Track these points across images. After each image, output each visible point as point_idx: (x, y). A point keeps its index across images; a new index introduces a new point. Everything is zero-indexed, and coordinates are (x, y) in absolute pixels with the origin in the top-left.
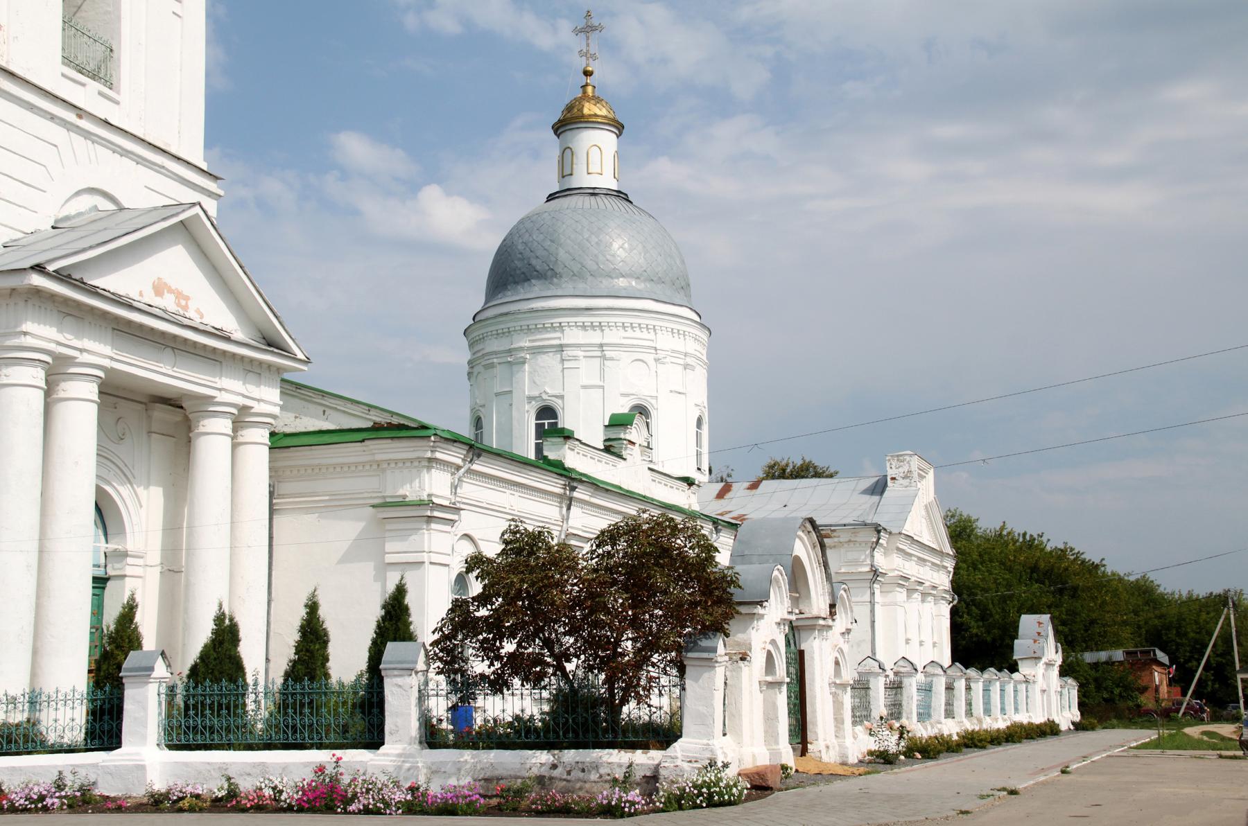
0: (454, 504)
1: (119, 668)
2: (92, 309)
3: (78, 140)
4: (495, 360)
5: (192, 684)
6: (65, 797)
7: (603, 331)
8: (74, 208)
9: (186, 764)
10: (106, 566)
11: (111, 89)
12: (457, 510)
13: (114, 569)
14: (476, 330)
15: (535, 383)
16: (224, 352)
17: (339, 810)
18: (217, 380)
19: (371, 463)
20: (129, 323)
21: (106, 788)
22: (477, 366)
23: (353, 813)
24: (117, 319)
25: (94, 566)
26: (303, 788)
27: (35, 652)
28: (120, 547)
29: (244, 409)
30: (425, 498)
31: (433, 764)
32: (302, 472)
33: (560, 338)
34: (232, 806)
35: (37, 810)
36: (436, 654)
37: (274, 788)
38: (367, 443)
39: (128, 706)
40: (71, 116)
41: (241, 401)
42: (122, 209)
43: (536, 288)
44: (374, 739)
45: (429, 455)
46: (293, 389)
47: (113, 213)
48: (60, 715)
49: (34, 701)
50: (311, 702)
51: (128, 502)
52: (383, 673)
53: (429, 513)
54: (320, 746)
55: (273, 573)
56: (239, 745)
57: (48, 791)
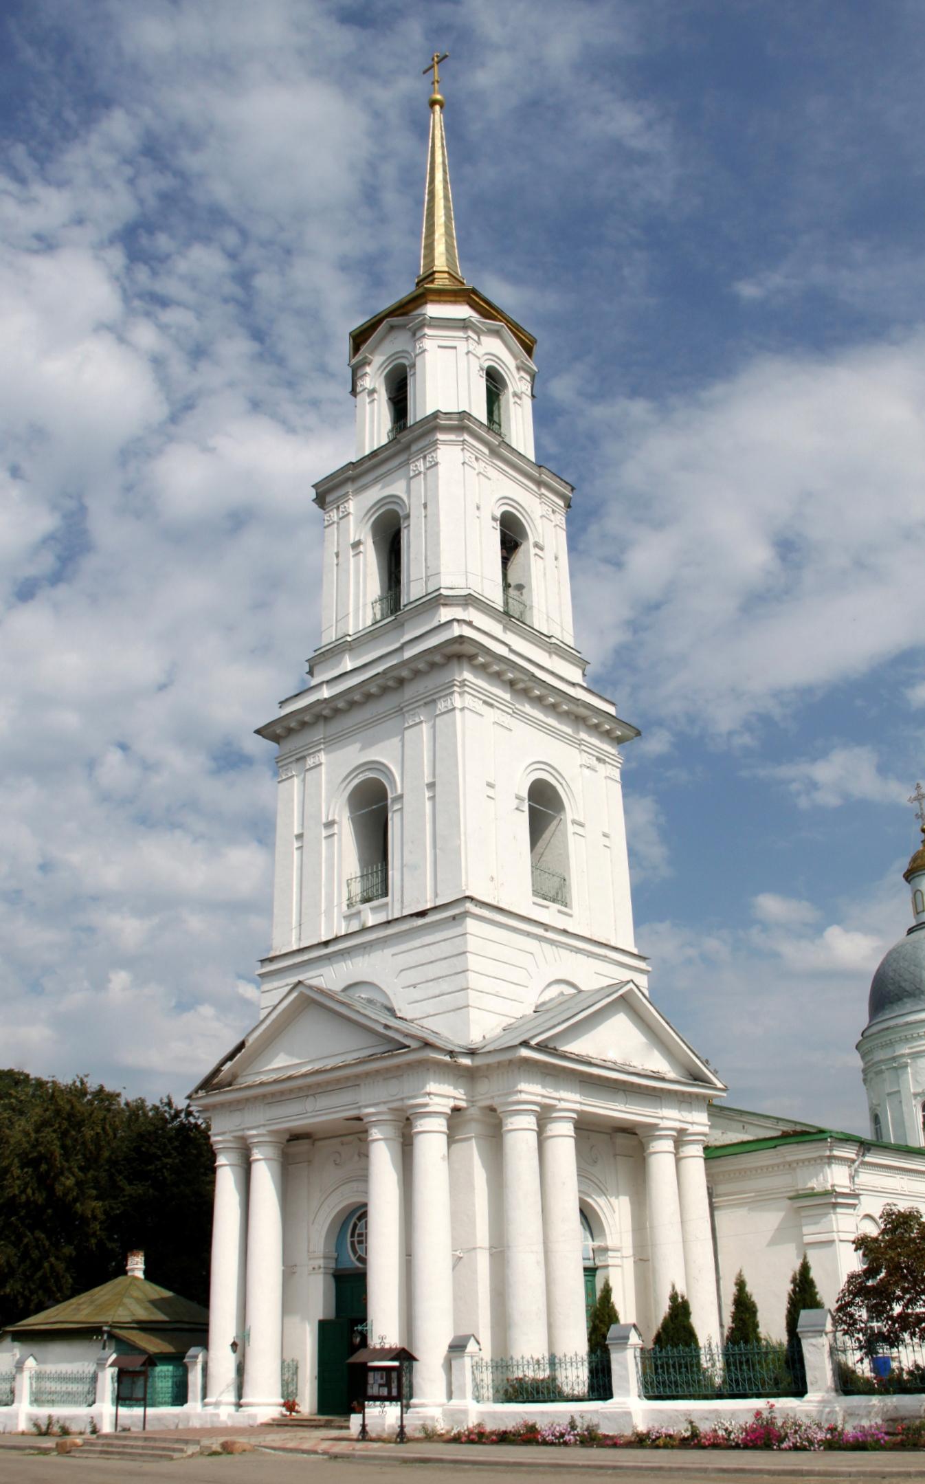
0: (854, 1191)
1: (604, 1337)
2: (564, 1069)
3: (546, 946)
4: (883, 1067)
5: (658, 1349)
6: (578, 1435)
8: (546, 996)
9: (661, 1411)
10: (594, 1259)
11: (566, 907)
12: (857, 1196)
13: (600, 1261)
14: (865, 1045)
15: (917, 1081)
16: (662, 1090)
17: (775, 1447)
18: (659, 1111)
19: (784, 1164)
20: (591, 1075)
21: (605, 1429)
22: (870, 1073)
23: (785, 1449)
24: (582, 1073)
25: (584, 1259)
26: (746, 1430)
27: (550, 1327)
28: (603, 1244)
29: (682, 1132)
30: (830, 1188)
31: (848, 1408)
32: (732, 1175)
34: (695, 1444)
35: (560, 1444)
36: (841, 1319)
37: (726, 1430)
38: (779, 1148)
39: (615, 1367)
40: (539, 931)
41: (678, 1125)
42: (580, 991)
43: (908, 1005)
44: (799, 1390)
45: (828, 1153)
46: (718, 1112)
47: (574, 996)
48: (569, 1374)
49: (553, 1362)
50: (747, 1361)
51: (605, 1210)
52: (800, 1336)
53: (833, 1200)
54: (759, 1396)
55: (720, 1257)
56: (699, 1395)
57: (566, 1430)
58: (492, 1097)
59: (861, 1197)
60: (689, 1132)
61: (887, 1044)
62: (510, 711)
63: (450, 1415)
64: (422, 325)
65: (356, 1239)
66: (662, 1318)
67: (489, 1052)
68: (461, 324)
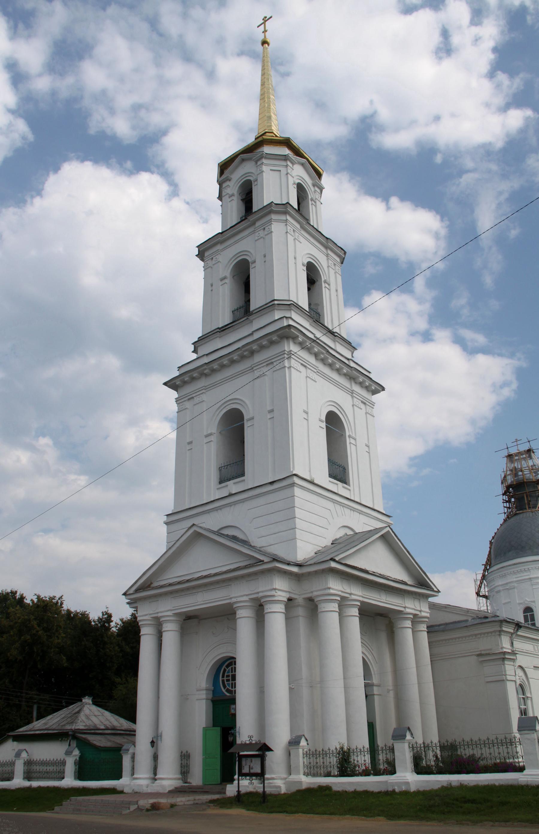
3: (338, 507)
7: (530, 571)
33: (529, 575)
58: (312, 592)
59: (517, 655)
60: (419, 616)
61: (503, 576)
62: (315, 371)
63: (289, 784)
64: (261, 157)
65: (225, 678)
66: (393, 729)
67: (310, 565)
68: (283, 158)
